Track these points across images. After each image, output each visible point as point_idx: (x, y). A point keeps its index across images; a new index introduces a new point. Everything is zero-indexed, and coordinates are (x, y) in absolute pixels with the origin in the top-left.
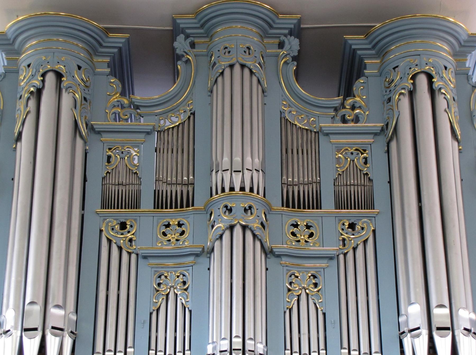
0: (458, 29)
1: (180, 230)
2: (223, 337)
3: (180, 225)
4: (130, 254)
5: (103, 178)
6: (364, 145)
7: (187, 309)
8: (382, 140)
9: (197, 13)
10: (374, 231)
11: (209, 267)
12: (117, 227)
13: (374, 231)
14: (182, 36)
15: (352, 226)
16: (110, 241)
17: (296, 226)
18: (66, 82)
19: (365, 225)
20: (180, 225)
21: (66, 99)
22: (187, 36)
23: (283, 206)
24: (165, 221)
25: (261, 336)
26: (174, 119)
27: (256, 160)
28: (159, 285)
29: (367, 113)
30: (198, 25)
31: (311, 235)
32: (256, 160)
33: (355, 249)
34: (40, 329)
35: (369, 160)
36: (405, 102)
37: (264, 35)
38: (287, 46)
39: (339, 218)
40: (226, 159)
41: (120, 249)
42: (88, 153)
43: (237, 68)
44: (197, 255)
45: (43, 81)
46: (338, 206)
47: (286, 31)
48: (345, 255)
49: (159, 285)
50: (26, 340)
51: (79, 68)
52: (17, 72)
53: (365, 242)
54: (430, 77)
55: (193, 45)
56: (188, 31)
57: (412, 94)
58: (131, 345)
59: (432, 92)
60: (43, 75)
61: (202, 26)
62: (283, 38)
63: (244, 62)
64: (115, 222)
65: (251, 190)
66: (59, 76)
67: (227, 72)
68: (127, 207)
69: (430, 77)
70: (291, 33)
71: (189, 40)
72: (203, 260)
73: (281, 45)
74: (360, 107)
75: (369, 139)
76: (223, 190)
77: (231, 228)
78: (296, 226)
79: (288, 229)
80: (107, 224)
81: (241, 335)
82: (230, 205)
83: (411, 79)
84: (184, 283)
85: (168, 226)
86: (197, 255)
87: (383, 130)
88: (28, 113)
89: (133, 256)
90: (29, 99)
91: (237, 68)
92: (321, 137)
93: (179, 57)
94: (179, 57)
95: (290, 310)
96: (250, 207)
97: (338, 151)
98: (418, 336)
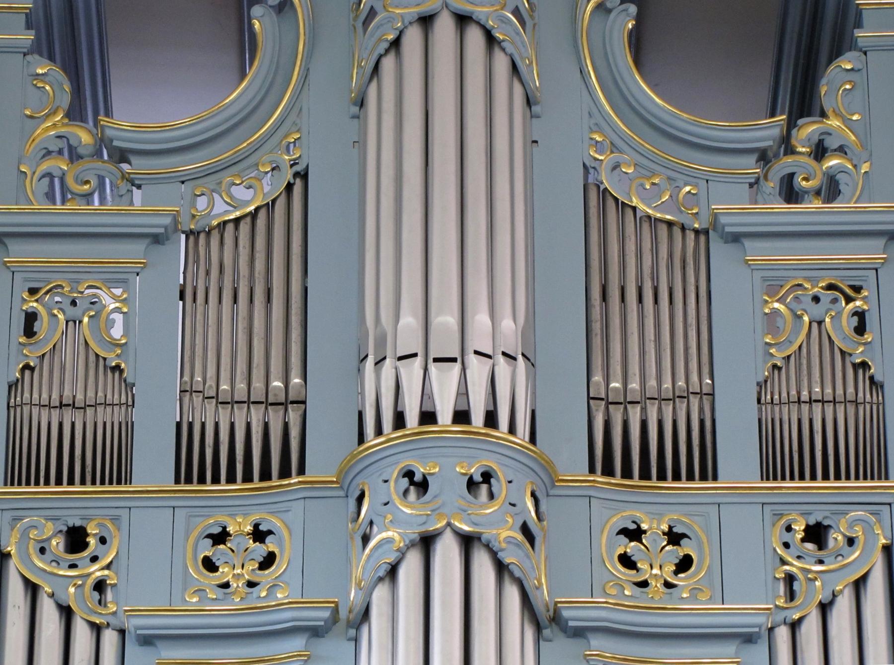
1: (260, 550)
4: (97, 629)
12: (58, 544)
16: (33, 589)
19: (858, 532)
20: (259, 535)
24: (621, 520)
26: (240, 192)
29: (865, 168)
31: (685, 564)
33: (825, 608)
35: (871, 321)
40: (410, 321)
41: (67, 613)
43: (445, 26)
44: (315, 632)
48: (794, 626)
53: (859, 585)
64: (49, 529)
65: (491, 419)
67: (413, 38)
74: (841, 150)
76: (399, 421)
77: (427, 542)
78: (635, 534)
82: (420, 470)
86: (315, 632)
89: (110, 638)
91: (445, 26)
92: (718, 248)
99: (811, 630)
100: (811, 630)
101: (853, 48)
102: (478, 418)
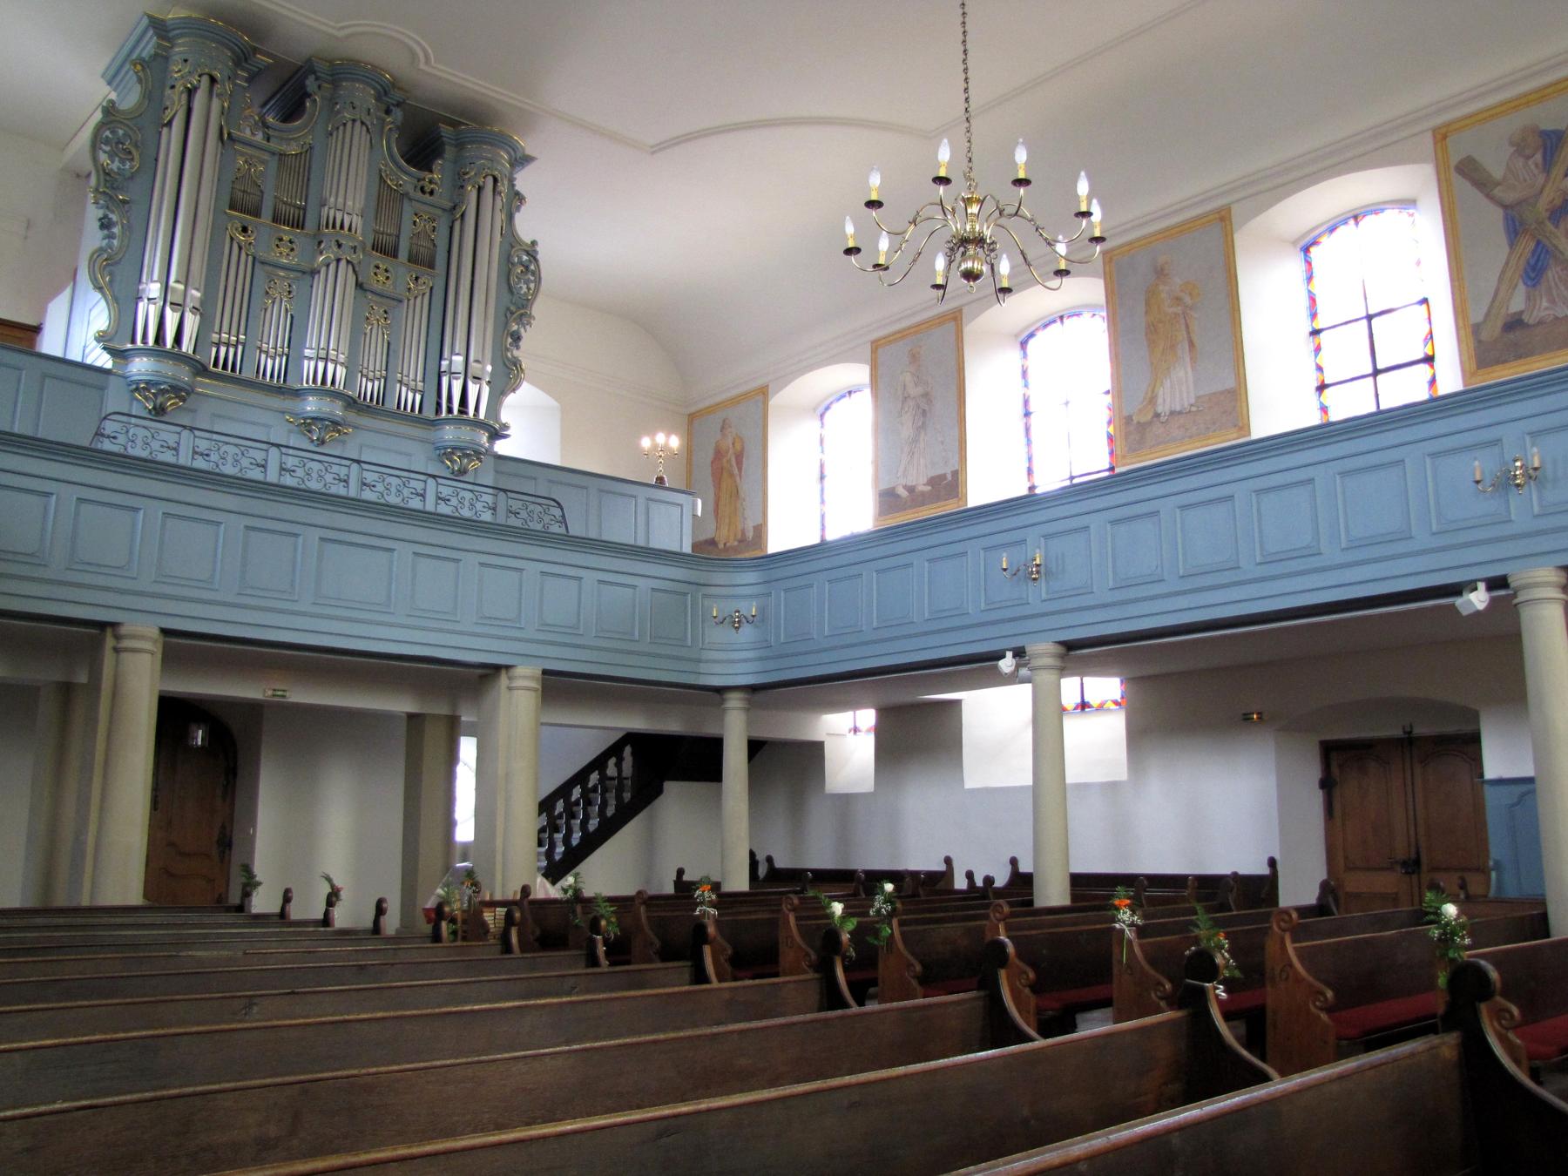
0: (518, 145)
3: (291, 242)
4: (247, 255)
5: (233, 182)
6: (1205, 491)
7: (289, 314)
10: (431, 288)
11: (957, 467)
13: (431, 288)
14: (313, 76)
17: (378, 267)
18: (217, 87)
19: (426, 281)
20: (291, 242)
21: (216, 103)
23: (373, 249)
25: (344, 347)
27: (357, 205)
29: (440, 190)
30: (329, 73)
33: (416, 298)
34: (463, 373)
35: (436, 230)
37: (378, 99)
40: (332, 199)
42: (534, 243)
44: (304, 273)
46: (275, 220)
47: (394, 102)
53: (424, 294)
54: (495, 180)
55: (319, 87)
56: (319, 74)
57: (480, 189)
58: (227, 331)
61: (332, 75)
63: (365, 121)
66: (213, 80)
67: (349, 125)
68: (295, 225)
71: (318, 83)
73: (388, 112)
74: (436, 184)
75: (439, 212)
77: (338, 260)
79: (373, 270)
80: (232, 226)
81: (326, 348)
82: (341, 241)
83: (484, 178)
84: (290, 292)
86: (304, 273)
89: (250, 258)
90: (182, 92)
91: (358, 124)
92: (406, 201)
93: (309, 95)
94: (309, 95)
98: (457, 379)
100: (412, 302)
101: (461, 408)
102: (353, 230)
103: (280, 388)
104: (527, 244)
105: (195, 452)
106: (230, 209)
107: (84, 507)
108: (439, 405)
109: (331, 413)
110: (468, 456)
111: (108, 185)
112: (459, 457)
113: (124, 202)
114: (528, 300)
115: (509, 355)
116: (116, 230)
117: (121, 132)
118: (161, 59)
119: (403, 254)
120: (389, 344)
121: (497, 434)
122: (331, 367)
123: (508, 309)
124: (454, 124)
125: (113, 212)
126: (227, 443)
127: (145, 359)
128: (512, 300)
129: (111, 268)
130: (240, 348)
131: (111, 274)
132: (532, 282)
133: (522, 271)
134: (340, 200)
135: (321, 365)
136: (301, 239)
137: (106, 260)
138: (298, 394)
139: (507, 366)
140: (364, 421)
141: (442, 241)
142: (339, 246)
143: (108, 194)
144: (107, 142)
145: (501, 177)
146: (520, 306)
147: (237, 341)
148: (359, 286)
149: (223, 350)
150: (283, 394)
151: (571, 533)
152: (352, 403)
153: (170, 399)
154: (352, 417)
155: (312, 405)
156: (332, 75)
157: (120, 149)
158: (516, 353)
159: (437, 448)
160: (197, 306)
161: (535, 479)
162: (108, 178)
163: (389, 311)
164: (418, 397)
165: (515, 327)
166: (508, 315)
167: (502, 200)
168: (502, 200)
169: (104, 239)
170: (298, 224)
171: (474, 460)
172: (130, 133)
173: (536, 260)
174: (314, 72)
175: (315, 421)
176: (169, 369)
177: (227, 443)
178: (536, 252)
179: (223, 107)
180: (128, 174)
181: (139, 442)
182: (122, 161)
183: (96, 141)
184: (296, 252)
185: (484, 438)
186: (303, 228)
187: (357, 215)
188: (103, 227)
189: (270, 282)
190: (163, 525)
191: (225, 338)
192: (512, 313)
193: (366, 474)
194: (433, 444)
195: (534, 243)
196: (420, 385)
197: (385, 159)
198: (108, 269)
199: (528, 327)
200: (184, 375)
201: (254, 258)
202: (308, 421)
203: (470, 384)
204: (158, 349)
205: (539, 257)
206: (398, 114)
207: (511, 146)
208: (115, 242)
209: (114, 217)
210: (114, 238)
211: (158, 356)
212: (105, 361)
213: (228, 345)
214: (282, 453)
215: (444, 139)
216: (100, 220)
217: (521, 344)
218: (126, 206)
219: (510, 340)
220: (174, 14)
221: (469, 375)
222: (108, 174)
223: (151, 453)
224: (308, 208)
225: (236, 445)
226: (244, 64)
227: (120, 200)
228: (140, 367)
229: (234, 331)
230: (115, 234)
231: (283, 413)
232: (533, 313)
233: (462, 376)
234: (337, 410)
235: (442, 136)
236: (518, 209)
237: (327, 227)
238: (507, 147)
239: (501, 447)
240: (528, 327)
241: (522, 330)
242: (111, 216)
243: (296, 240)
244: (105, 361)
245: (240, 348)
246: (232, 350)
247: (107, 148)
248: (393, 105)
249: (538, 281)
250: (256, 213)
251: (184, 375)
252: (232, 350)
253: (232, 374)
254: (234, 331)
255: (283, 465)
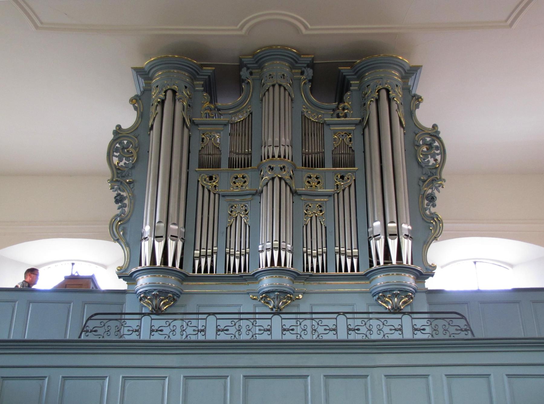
0: (403, 63)
1: (243, 180)
2: (268, 241)
3: (243, 177)
4: (215, 194)
8: (360, 128)
9: (254, 54)
10: (355, 180)
13: (355, 180)
14: (245, 69)
15: (342, 177)
17: (310, 177)
19: (350, 177)
20: (243, 177)
22: (248, 68)
24: (235, 175)
25: (289, 240)
26: (240, 116)
27: (288, 140)
28: (231, 211)
31: (319, 183)
32: (288, 140)
33: (344, 190)
34: (164, 237)
36: (374, 106)
38: (306, 74)
39: (335, 173)
40: (270, 139)
41: (209, 191)
42: (435, 126)
45: (165, 95)
48: (338, 194)
49: (231, 211)
50: (156, 243)
51: (186, 87)
52: (150, 90)
53: (350, 186)
54: (388, 91)
55: (251, 74)
56: (249, 65)
57: (377, 101)
59: (389, 100)
60: (166, 92)
61: (257, 63)
62: (303, 69)
64: (206, 176)
65: (285, 157)
66: (174, 92)
67: (271, 89)
68: (319, 166)
69: (388, 91)
70: (308, 66)
71: (249, 71)
72: (257, 197)
78: (310, 177)
79: (305, 180)
80: (202, 177)
84: (246, 210)
85: (236, 178)
87: (361, 122)
88: (157, 113)
89: (217, 196)
90: (157, 106)
91: (277, 87)
92: (325, 126)
93: (243, 81)
94: (243, 81)
95: (307, 225)
96: (284, 167)
97: (335, 134)
98: (379, 239)
99: (341, 194)
100: (341, 194)
102: (282, 157)
103: (241, 276)
104: (428, 129)
105: (349, 330)
106: (199, 168)
107: (68, 383)
108: (371, 262)
109: (280, 285)
110: (396, 295)
111: (119, 176)
112: (389, 297)
113: (130, 183)
114: (436, 168)
115: (427, 212)
116: (126, 202)
117: (125, 142)
118: (146, 91)
119: (328, 161)
120: (326, 228)
121: (429, 272)
122: (283, 253)
123: (420, 179)
124: (351, 64)
125: (123, 191)
126: (436, 319)
127: (145, 276)
128: (422, 172)
129: (124, 225)
130: (324, 255)
131: (124, 230)
132: (438, 154)
133: (427, 149)
134: (277, 139)
135: (276, 253)
136: (249, 174)
137: (120, 221)
138: (255, 277)
139: (425, 221)
140: (313, 286)
141: (357, 146)
142: (272, 169)
143: (119, 181)
144: (117, 150)
145: (392, 89)
146: (430, 174)
147: (212, 252)
148: (294, 193)
149: (203, 260)
150: (245, 280)
151: (477, 336)
152: (296, 276)
153: (162, 300)
154: (299, 286)
155: (266, 283)
156: (257, 63)
157: (124, 152)
158: (433, 210)
159: (374, 296)
160: (407, 234)
161: (467, 304)
162: (119, 172)
163: (322, 205)
164: (355, 261)
165: (430, 191)
166: (421, 183)
167: (397, 103)
168: (397, 103)
169: (119, 209)
170: (247, 164)
171: (403, 298)
172: (131, 140)
173: (439, 139)
174: (245, 66)
175: (268, 295)
176: (159, 280)
177: (436, 319)
178: (438, 133)
179: (184, 106)
180: (130, 166)
181: (375, 330)
182: (127, 159)
183: (111, 150)
184: (247, 183)
185: (410, 280)
186: (251, 166)
187: (288, 146)
188: (117, 202)
189: (307, 206)
190: (326, 386)
191: (355, 252)
192: (424, 181)
193: (415, 322)
194: (371, 293)
195: (435, 126)
196: (355, 251)
197: (305, 104)
198: (121, 227)
199: (440, 188)
200: (172, 283)
201: (219, 195)
202: (264, 295)
203: (170, 241)
204: (152, 269)
205: (440, 135)
206: (309, 72)
207: (400, 65)
208: (126, 209)
209: (124, 194)
210: (126, 207)
211: (155, 272)
212: (122, 285)
213: (206, 256)
214: (217, 319)
215: (347, 77)
216: (115, 197)
217: (437, 202)
218: (132, 185)
219: (426, 202)
220: (144, 64)
221: (388, 235)
222: (119, 169)
223: (384, 336)
224: (325, 152)
225: (378, 319)
226: (297, 65)
227: (127, 183)
228: (143, 282)
229: (315, 247)
230: (126, 204)
231: (248, 293)
232: (443, 177)
233: (382, 237)
234: (286, 282)
235: (345, 76)
236: (417, 107)
237: (265, 159)
238: (395, 66)
239: (430, 284)
240: (440, 188)
241: (436, 191)
242: (122, 193)
243: (246, 175)
244: (122, 285)
245: (324, 255)
246: (209, 259)
247: (117, 154)
248: (305, 67)
249: (443, 153)
250: (218, 165)
251: (172, 283)
252: (209, 259)
253: (206, 275)
254: (315, 247)
255: (415, 326)
